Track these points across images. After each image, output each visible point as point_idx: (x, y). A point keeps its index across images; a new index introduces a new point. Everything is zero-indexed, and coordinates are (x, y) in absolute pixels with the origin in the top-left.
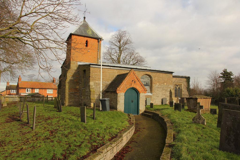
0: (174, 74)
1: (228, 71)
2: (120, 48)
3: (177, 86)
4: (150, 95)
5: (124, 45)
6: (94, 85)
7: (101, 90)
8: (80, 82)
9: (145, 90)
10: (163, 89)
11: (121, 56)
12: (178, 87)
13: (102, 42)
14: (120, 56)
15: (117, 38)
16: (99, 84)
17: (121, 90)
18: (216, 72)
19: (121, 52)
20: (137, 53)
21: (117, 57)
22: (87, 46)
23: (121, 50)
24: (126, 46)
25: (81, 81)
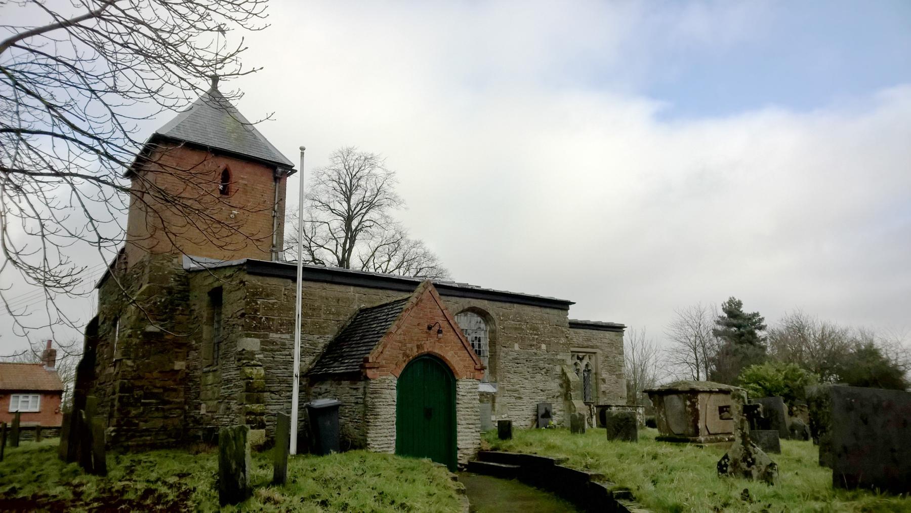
0: (574, 314)
1: (746, 310)
2: (349, 220)
3: (578, 361)
4: (488, 393)
5: (364, 211)
6: (263, 350)
7: (296, 370)
8: (194, 342)
9: (478, 366)
10: (537, 369)
11: (354, 250)
12: (585, 362)
13: (292, 182)
14: (348, 251)
15: (339, 183)
16: (287, 347)
17: (382, 367)
18: (700, 315)
19: (351, 236)
20: (416, 243)
21: (336, 254)
22: (225, 192)
23: (353, 228)
24: (373, 214)
25: (199, 340)
